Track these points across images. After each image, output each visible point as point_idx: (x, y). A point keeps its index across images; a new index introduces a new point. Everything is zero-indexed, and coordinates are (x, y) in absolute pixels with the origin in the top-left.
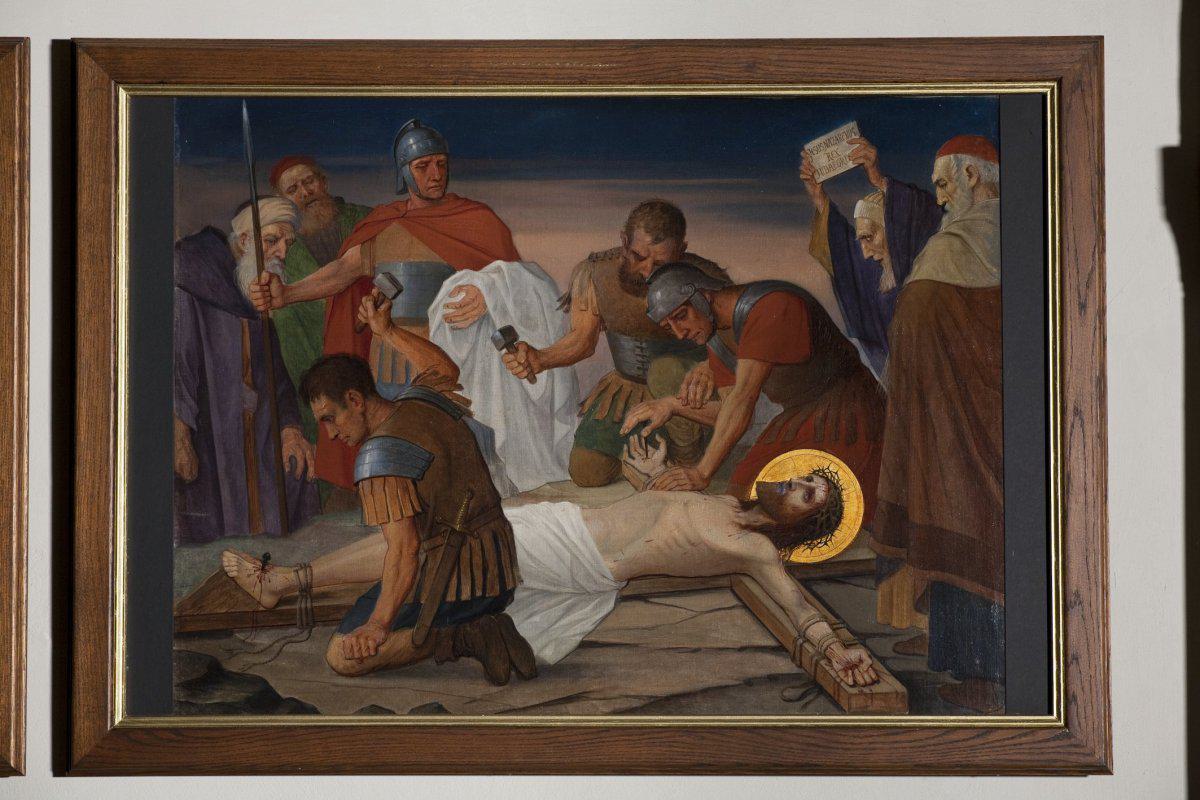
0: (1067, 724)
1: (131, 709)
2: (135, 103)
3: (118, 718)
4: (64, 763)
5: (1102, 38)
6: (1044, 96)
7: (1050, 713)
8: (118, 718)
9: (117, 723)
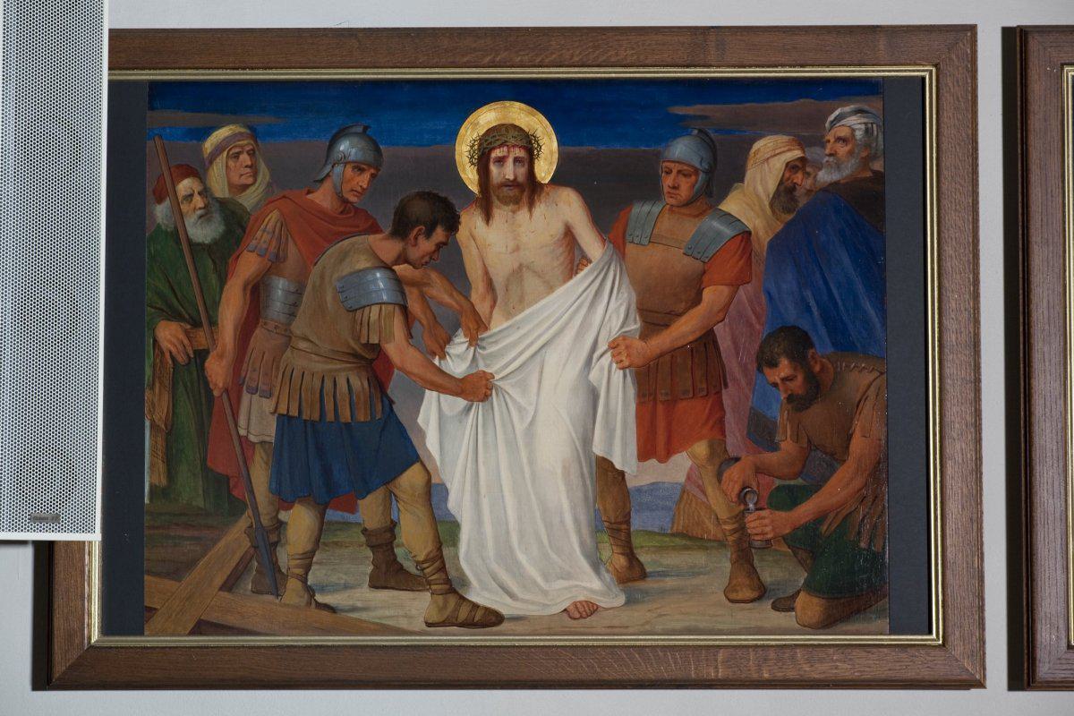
0: (944, 645)
1: (107, 629)
4: (1023, 675)
5: (972, 29)
6: (923, 79)
7: (930, 632)
9: (93, 641)
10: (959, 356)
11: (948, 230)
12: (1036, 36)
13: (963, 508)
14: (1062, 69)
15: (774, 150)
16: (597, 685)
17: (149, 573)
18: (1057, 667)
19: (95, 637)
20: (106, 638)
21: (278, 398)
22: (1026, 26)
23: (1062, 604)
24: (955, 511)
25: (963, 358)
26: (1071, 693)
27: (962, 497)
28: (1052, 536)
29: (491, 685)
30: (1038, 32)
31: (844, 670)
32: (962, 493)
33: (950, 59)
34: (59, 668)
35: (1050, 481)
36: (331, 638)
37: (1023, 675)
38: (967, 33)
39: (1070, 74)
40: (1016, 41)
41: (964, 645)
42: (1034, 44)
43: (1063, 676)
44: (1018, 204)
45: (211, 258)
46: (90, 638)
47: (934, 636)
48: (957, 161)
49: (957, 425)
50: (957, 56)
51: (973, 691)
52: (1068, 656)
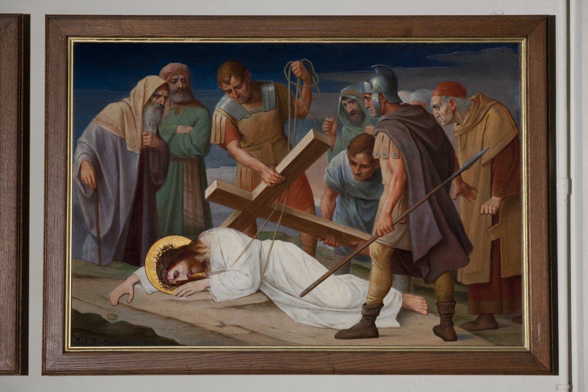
1: (516, 47)
10: (8, 194)
11: (4, 125)
12: (54, 21)
13: (8, 277)
14: (67, 39)
18: (57, 363)
19: (523, 43)
20: (518, 41)
23: (60, 327)
24: (4, 278)
25: (11, 195)
27: (8, 271)
28: (56, 292)
30: (54, 18)
31: (53, 171)
32: (8, 269)
33: (6, 32)
34: (542, 27)
35: (56, 263)
39: (72, 41)
40: (22, 368)
41: (7, 352)
43: (60, 368)
44: (22, 316)
48: (9, 88)
49: (6, 232)
50: (10, 31)
52: (63, 357)
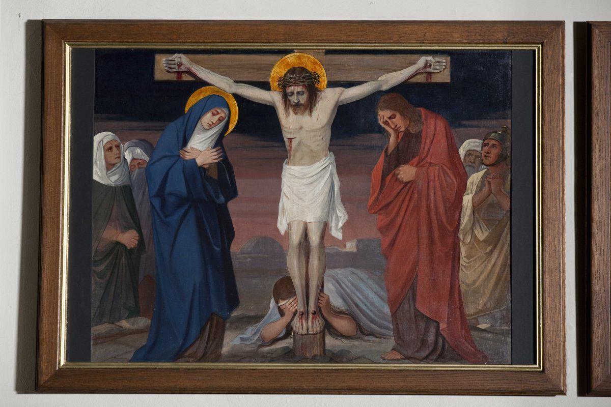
1: (69, 358)
2: (74, 53)
3: (62, 363)
4: (585, 388)
6: (534, 51)
7: (535, 363)
8: (62, 363)
9: (61, 366)
15: (275, 40)
16: (548, 393)
17: (503, 333)
21: (397, 234)
22: (590, 22)
26: (610, 398)
29: (502, 393)
36: (318, 365)
37: (585, 388)
38: (560, 25)
40: (578, 26)
42: (595, 33)
45: (465, 171)
46: (59, 363)
47: (538, 365)
51: (557, 397)
